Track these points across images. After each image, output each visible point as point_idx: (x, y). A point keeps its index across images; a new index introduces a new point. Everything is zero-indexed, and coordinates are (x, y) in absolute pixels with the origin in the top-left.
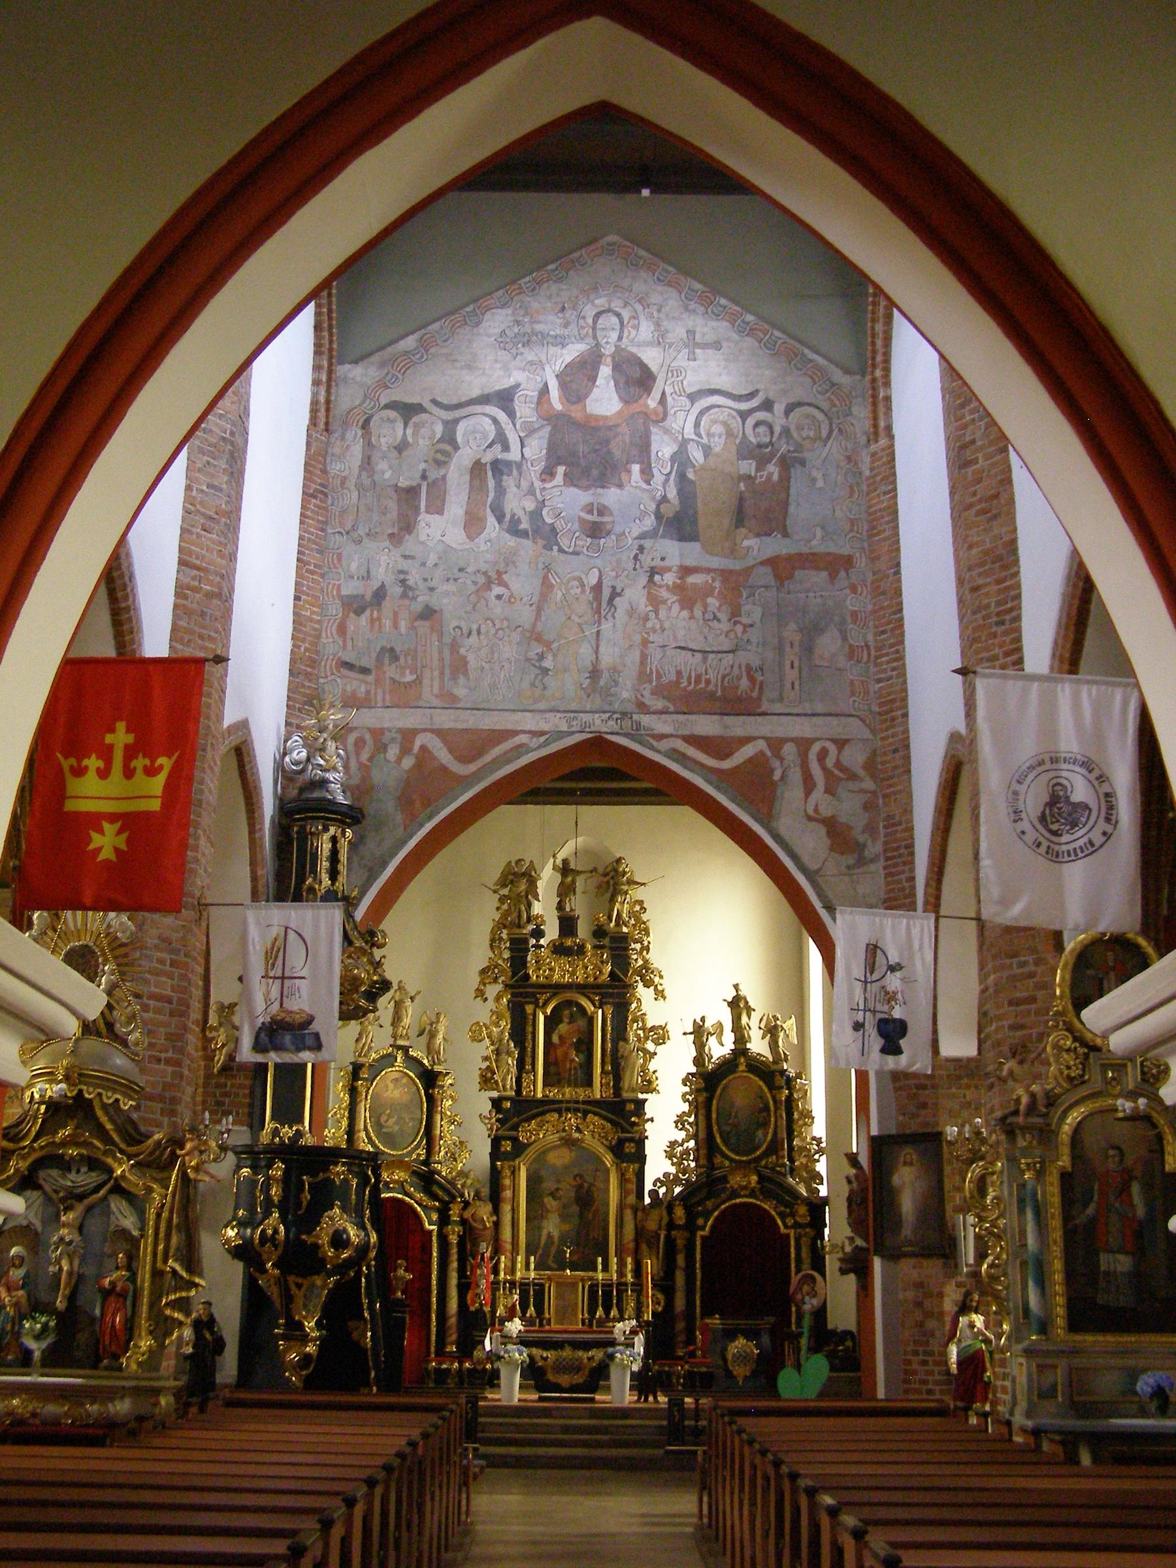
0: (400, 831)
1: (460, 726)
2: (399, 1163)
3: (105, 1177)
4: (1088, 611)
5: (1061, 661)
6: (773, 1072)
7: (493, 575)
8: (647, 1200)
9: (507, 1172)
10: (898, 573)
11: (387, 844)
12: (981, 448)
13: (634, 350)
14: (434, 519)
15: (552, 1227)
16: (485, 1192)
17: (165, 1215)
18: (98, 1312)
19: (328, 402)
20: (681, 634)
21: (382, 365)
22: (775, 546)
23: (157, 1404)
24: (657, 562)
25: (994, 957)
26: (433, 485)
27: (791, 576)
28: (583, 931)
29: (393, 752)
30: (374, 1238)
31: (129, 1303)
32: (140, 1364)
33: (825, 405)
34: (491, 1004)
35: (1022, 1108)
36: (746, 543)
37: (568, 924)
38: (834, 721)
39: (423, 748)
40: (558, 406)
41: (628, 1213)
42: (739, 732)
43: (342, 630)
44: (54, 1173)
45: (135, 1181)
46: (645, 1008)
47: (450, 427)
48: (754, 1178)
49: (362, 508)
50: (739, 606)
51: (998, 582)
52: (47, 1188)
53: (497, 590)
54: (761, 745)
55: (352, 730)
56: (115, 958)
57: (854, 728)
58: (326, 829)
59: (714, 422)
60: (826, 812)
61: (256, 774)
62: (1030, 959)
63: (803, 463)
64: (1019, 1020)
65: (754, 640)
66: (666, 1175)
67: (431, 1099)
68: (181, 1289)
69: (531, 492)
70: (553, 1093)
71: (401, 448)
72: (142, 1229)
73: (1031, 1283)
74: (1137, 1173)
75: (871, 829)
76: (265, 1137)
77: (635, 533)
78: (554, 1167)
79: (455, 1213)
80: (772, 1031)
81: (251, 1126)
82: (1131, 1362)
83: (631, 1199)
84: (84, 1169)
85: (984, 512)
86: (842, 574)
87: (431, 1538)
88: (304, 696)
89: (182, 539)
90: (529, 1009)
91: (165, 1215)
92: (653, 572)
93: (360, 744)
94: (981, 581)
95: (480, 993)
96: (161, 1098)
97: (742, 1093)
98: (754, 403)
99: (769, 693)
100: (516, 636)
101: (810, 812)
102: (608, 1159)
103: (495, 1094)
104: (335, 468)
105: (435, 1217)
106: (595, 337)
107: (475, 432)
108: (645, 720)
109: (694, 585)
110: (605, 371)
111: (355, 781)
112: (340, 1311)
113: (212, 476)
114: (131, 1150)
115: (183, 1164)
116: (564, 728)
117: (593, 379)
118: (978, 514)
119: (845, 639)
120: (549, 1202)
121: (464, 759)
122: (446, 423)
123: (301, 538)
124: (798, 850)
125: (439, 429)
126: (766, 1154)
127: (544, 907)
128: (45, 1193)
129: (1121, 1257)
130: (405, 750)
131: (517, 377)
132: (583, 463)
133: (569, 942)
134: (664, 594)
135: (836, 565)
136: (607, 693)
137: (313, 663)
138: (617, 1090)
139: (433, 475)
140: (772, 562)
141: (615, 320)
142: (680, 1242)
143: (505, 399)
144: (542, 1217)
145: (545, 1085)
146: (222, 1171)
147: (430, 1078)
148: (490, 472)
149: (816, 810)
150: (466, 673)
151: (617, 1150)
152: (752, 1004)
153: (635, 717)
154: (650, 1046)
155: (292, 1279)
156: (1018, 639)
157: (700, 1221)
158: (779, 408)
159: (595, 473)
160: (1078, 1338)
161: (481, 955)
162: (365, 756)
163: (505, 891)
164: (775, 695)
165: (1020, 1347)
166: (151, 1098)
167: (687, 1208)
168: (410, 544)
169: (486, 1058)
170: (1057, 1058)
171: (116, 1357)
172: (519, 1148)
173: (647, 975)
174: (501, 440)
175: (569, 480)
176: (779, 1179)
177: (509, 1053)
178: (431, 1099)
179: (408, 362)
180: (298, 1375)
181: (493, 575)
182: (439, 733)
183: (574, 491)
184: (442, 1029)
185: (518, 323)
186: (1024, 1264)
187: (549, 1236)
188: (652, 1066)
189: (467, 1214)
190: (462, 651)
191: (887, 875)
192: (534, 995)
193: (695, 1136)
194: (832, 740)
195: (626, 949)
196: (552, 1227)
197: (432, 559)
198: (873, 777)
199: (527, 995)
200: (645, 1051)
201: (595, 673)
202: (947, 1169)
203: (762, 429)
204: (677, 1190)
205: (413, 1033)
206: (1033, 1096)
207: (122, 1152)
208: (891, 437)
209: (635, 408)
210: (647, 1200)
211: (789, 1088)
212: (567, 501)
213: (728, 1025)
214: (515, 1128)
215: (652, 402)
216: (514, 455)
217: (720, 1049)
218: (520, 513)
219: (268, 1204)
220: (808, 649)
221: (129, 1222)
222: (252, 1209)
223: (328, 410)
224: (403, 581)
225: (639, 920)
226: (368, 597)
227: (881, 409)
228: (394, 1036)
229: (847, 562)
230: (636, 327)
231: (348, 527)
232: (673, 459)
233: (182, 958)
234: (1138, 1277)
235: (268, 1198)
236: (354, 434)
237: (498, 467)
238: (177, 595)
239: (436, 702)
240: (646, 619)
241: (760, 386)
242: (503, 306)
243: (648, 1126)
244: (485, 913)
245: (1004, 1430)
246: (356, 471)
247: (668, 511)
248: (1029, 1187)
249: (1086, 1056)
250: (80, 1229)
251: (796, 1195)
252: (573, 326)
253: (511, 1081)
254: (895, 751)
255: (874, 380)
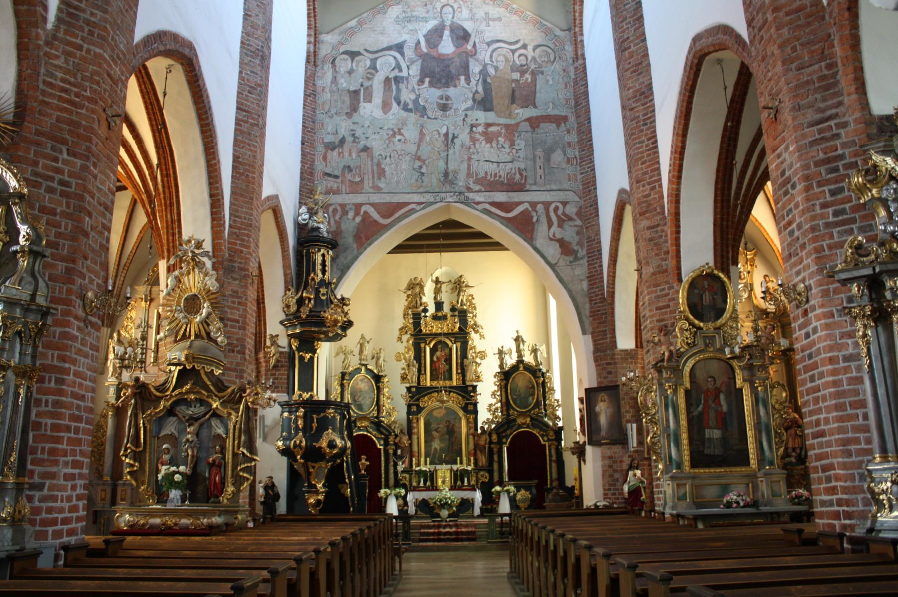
0: (355, 252)
1: (382, 201)
2: (364, 418)
3: (208, 409)
4: (691, 109)
5: (678, 135)
6: (536, 371)
7: (396, 130)
8: (480, 431)
9: (415, 421)
10: (590, 122)
11: (349, 258)
12: (631, 42)
13: (460, 23)
14: (367, 105)
15: (436, 445)
16: (405, 431)
17: (238, 426)
18: (207, 475)
19: (315, 52)
20: (487, 154)
21: (340, 34)
22: (530, 112)
23: (237, 518)
24: (474, 122)
25: (648, 287)
26: (366, 89)
27: (538, 126)
28: (446, 309)
29: (351, 215)
30: (349, 444)
31: (222, 470)
32: (228, 499)
33: (552, 46)
34: (405, 344)
35: (666, 358)
36: (516, 111)
37: (439, 306)
38: (561, 193)
39: (365, 212)
40: (424, 50)
41: (471, 437)
42: (516, 200)
43: (325, 158)
44: (183, 407)
45: (224, 412)
46: (475, 343)
47: (374, 61)
48: (528, 419)
49: (333, 102)
50: (514, 141)
51: (643, 104)
52: (180, 415)
53: (398, 137)
54: (526, 206)
55: (331, 205)
56: (209, 300)
57: (570, 196)
58: (319, 250)
59: (499, 55)
60: (558, 236)
61: (285, 226)
62: (666, 286)
63: (542, 73)
64: (661, 317)
65: (522, 156)
66: (488, 419)
67: (379, 389)
68: (248, 462)
69: (413, 90)
70: (434, 384)
71: (350, 72)
72: (227, 434)
73: (672, 444)
74: (724, 388)
75: (580, 243)
76: (295, 397)
77: (464, 107)
78: (436, 417)
79: (391, 439)
80: (535, 351)
81: (288, 393)
82: (723, 482)
83: (472, 431)
84: (198, 405)
85: (634, 71)
86: (563, 124)
87: (375, 579)
88: (306, 192)
89: (238, 97)
90: (422, 345)
91: (238, 426)
92: (472, 126)
93: (335, 211)
94: (634, 105)
95: (400, 339)
96: (235, 370)
97: (521, 380)
98: (518, 46)
99: (530, 181)
100: (408, 158)
101: (551, 236)
102: (461, 413)
103: (408, 385)
104: (319, 83)
105: (382, 442)
106: (441, 17)
107: (386, 64)
108: (471, 195)
109: (492, 132)
110: (447, 33)
111: (334, 228)
112: (334, 478)
113: (253, 67)
114: (219, 394)
115: (246, 400)
116: (432, 200)
117: (441, 37)
118: (631, 73)
119: (565, 155)
120: (435, 434)
121: (384, 217)
122: (372, 60)
123: (304, 115)
124: (546, 255)
125: (368, 63)
126: (533, 408)
127: (428, 299)
128: (179, 418)
129: (716, 431)
130: (357, 213)
131: (405, 37)
132: (437, 76)
133: (439, 314)
134: (478, 136)
135: (559, 120)
136: (452, 183)
137: (311, 174)
138: (464, 381)
139: (366, 84)
140: (528, 120)
141: (450, 9)
142: (495, 450)
143: (399, 48)
144: (432, 441)
145: (431, 380)
146: (272, 414)
147: (378, 378)
148: (393, 82)
149: (554, 235)
150: (384, 177)
151: (465, 409)
152: (525, 339)
153: (466, 194)
154: (478, 360)
155: (310, 464)
156: (655, 131)
157: (504, 440)
158: (530, 48)
159: (443, 81)
160: (697, 471)
161: (400, 322)
162: (337, 217)
163: (409, 292)
164: (533, 182)
165: (669, 476)
166: (230, 370)
167: (498, 434)
168: (356, 118)
169: (403, 369)
170: (682, 334)
171: (218, 497)
172: (420, 409)
173: (476, 327)
174: (398, 67)
175: (431, 84)
176: (539, 418)
177: (413, 366)
178: (379, 389)
179: (352, 32)
180: (314, 509)
181: (396, 130)
182: (372, 205)
183: (433, 90)
184: (382, 355)
185: (404, 12)
186: (668, 435)
187: (435, 449)
188: (480, 369)
189: (397, 440)
190: (383, 166)
191: (589, 265)
192: (424, 339)
193: (501, 401)
194: (561, 202)
195: (466, 316)
196: (436, 445)
197: (367, 123)
198: (581, 219)
199: (421, 339)
200: (477, 363)
201: (446, 174)
202: (622, 402)
203: (522, 58)
204: (493, 426)
205: (369, 357)
206: (671, 352)
207: (216, 396)
208: (584, 59)
209: (462, 50)
210: (480, 431)
211: (543, 377)
212: (430, 95)
213: (514, 349)
214: (418, 400)
215: (470, 47)
216: (404, 74)
217: (511, 361)
218: (408, 101)
219: (297, 428)
220: (548, 159)
221: (220, 431)
222: (290, 432)
223: (315, 56)
224: (353, 135)
225: (471, 304)
226: (337, 143)
227: (579, 46)
228: (360, 360)
229: (565, 119)
230: (461, 12)
231: (326, 110)
232: (480, 73)
233: (244, 301)
234: (724, 440)
235: (297, 426)
236: (328, 67)
237: (397, 80)
238: (237, 124)
239: (371, 191)
240: (470, 148)
241: (521, 38)
242: (398, 4)
243: (479, 397)
244: (401, 302)
245: (661, 517)
246: (329, 83)
247: (479, 97)
248: (670, 397)
249: (696, 332)
250: (197, 435)
251: (547, 425)
252: (431, 13)
253: (415, 378)
254: (591, 206)
255: (575, 33)
